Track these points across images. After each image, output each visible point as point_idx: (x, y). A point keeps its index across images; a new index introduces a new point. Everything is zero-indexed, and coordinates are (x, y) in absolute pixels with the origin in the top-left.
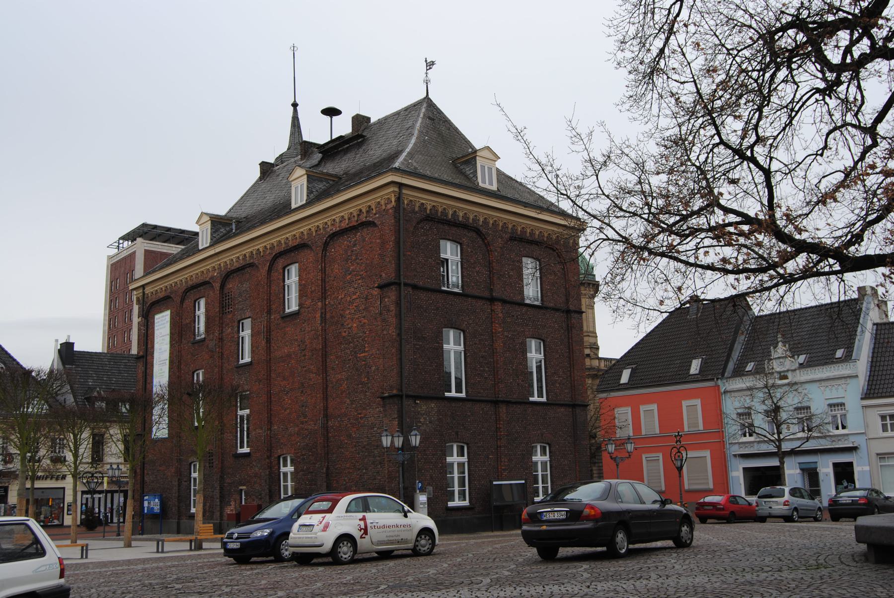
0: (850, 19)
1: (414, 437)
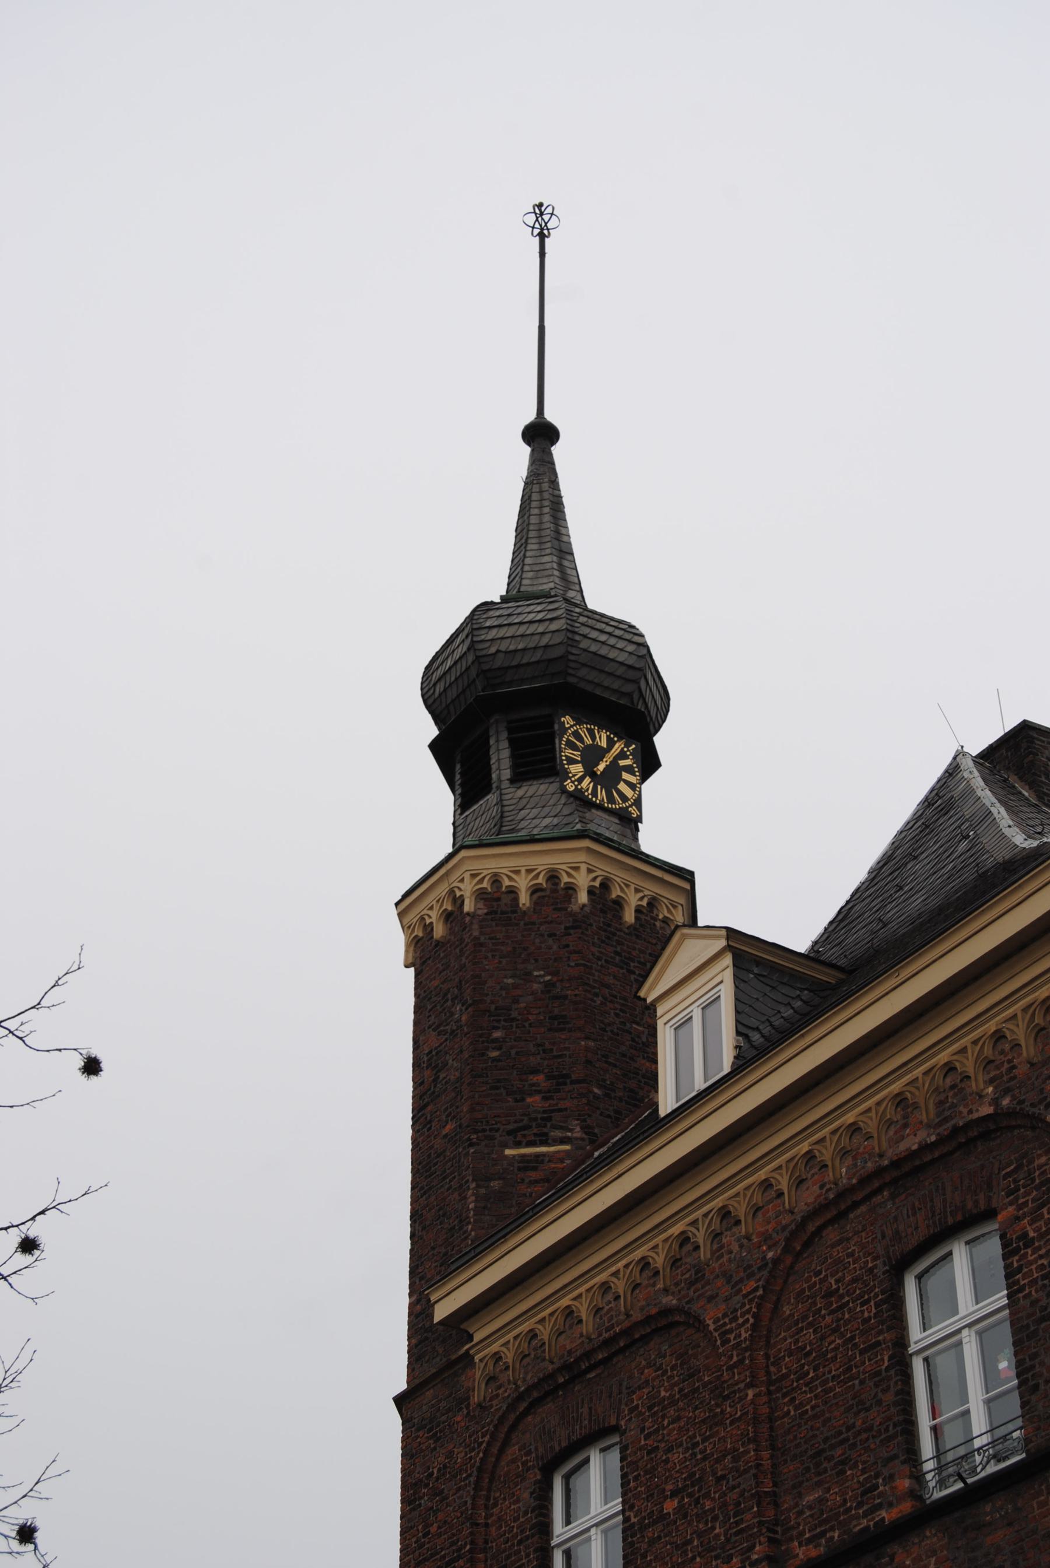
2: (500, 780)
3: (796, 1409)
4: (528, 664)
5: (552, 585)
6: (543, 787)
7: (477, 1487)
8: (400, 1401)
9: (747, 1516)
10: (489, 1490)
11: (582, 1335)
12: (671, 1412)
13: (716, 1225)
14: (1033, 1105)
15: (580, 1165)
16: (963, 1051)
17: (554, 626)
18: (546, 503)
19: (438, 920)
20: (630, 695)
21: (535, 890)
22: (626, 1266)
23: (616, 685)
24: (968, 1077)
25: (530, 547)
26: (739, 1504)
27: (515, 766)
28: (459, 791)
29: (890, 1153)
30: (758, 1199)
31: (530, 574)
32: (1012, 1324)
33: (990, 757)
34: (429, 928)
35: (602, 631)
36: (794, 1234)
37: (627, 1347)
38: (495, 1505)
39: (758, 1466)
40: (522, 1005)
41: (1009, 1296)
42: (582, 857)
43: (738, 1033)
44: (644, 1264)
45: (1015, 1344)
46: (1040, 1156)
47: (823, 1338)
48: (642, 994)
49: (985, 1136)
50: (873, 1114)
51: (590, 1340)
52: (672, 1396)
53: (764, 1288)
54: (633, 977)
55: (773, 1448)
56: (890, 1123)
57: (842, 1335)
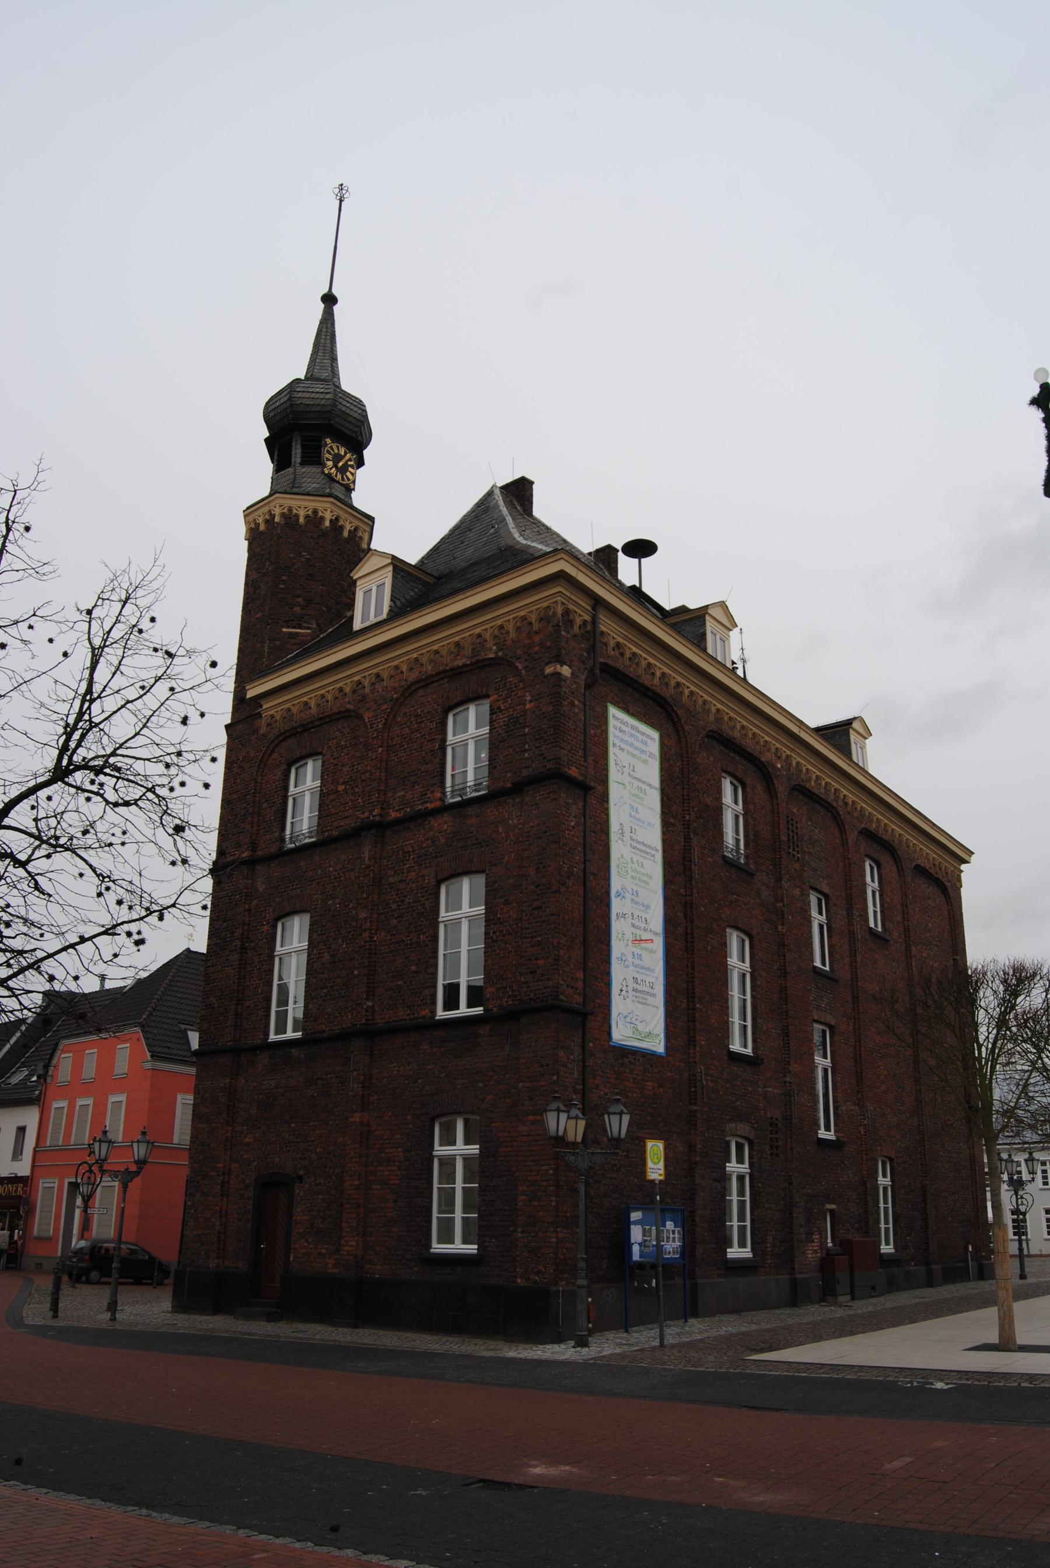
0: (493, 898)
1: (618, 1117)
2: (295, 463)
3: (398, 759)
4: (313, 412)
5: (327, 374)
6: (314, 469)
7: (259, 767)
8: (227, 727)
9: (373, 797)
10: (264, 769)
11: (310, 714)
12: (345, 751)
13: (373, 680)
14: (511, 658)
15: (313, 640)
16: (486, 630)
17: (328, 396)
18: (329, 334)
19: (262, 522)
20: (356, 432)
21: (307, 517)
22: (333, 689)
23: (351, 427)
24: (486, 641)
25: (319, 354)
26: (370, 792)
27: (303, 457)
28: (276, 463)
29: (450, 665)
30: (392, 672)
31: (318, 367)
32: (490, 741)
33: (506, 488)
34: (258, 525)
35: (348, 402)
36: (406, 689)
37: (329, 722)
38: (266, 775)
39: (380, 779)
40: (296, 567)
41: (490, 730)
42: (329, 505)
43: (391, 600)
44: (341, 690)
45: (490, 749)
46: (510, 678)
47: (412, 733)
48: (351, 575)
49: (490, 665)
50: (445, 648)
51: (314, 716)
52: (346, 744)
53: (391, 709)
54: (344, 561)
55: (387, 772)
56: (452, 653)
57: (420, 733)
